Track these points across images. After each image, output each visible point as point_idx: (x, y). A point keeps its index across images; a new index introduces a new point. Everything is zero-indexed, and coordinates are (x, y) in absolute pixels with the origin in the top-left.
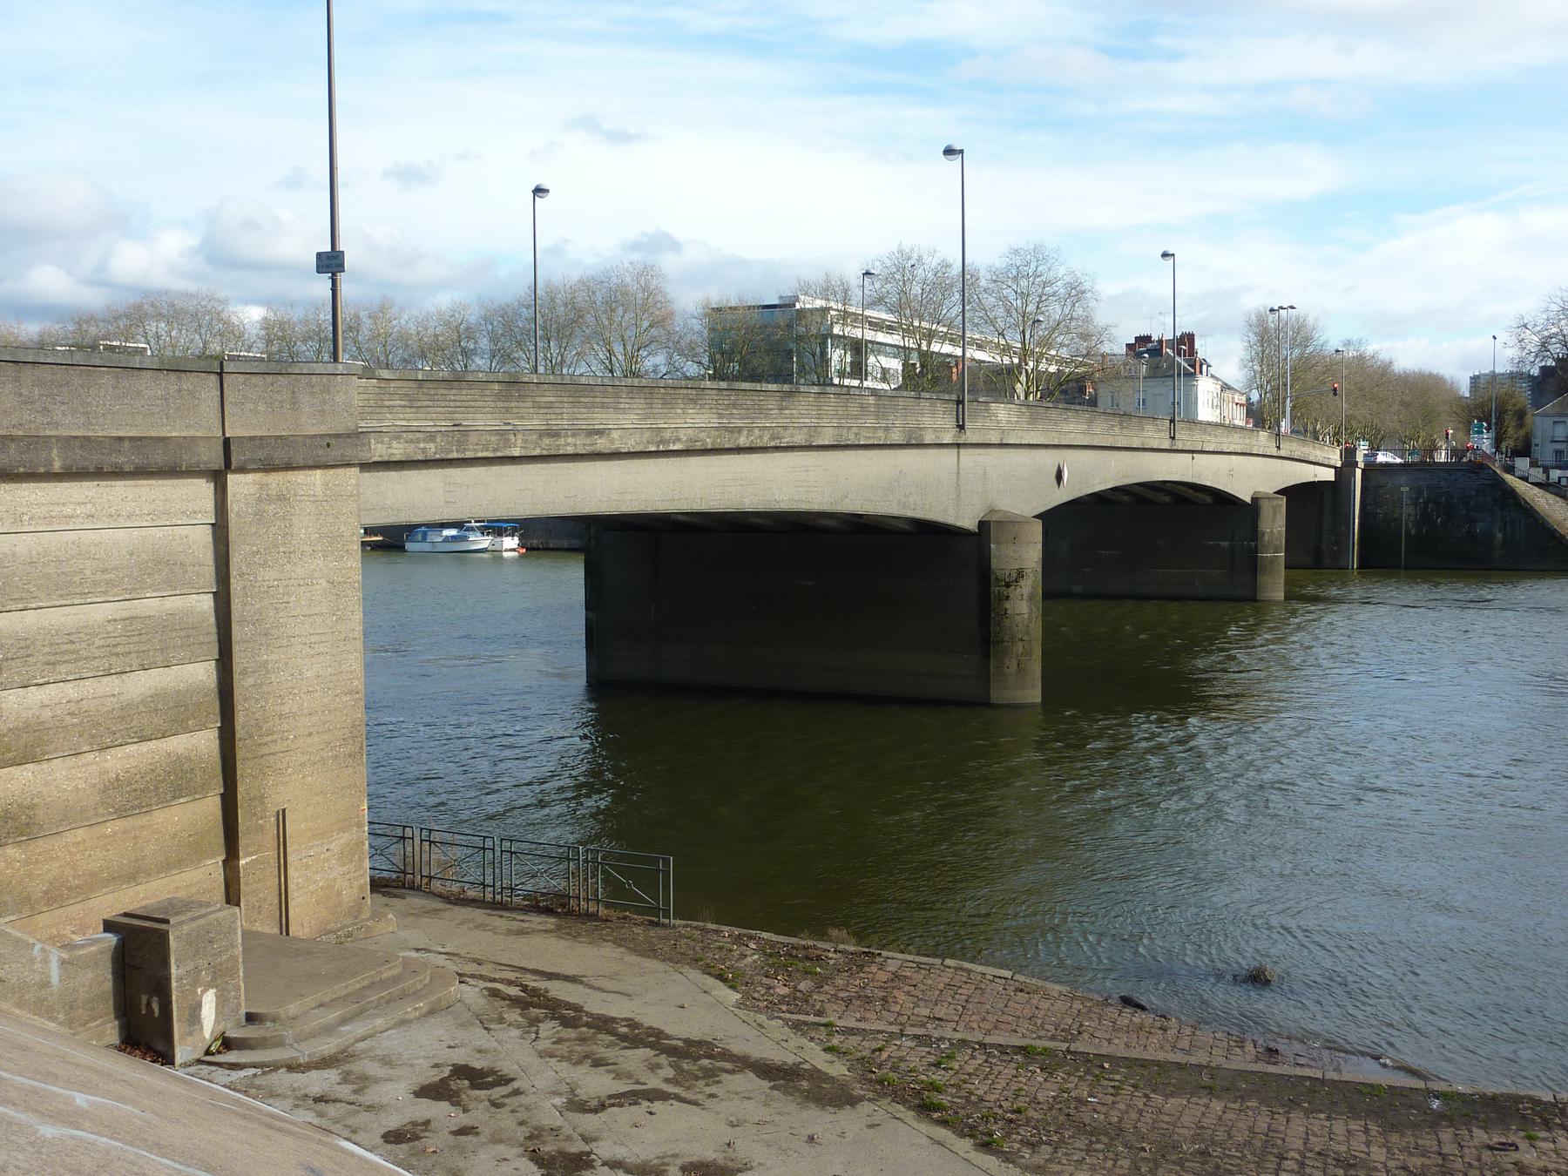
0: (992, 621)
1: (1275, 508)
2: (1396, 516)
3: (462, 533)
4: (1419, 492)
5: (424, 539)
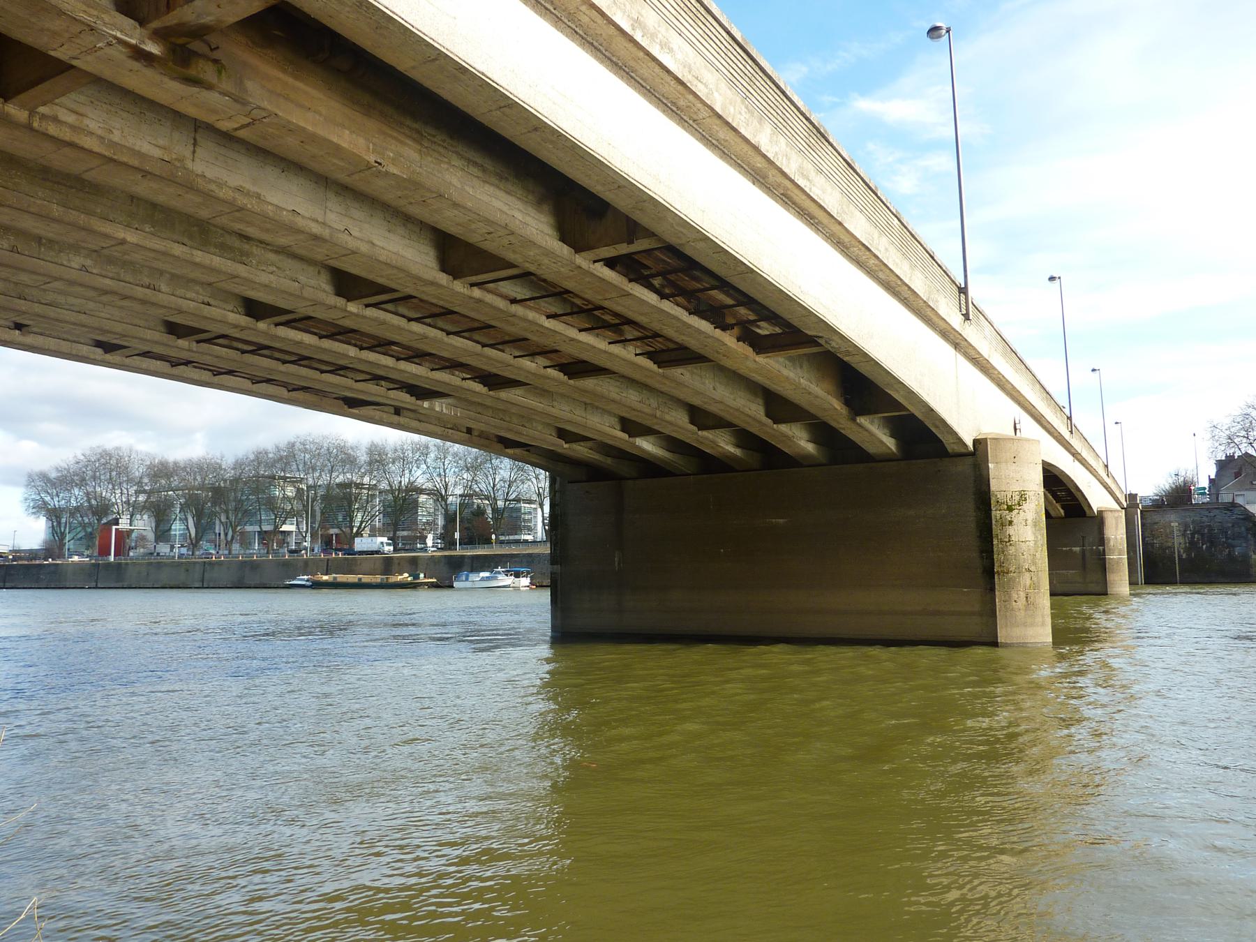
0: (995, 549)
1: (1117, 519)
2: (1170, 544)
3: (492, 575)
4: (1186, 526)
5: (467, 579)
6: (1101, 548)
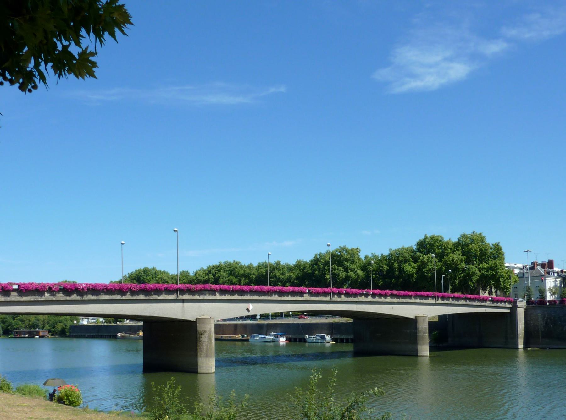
6: (416, 331)
